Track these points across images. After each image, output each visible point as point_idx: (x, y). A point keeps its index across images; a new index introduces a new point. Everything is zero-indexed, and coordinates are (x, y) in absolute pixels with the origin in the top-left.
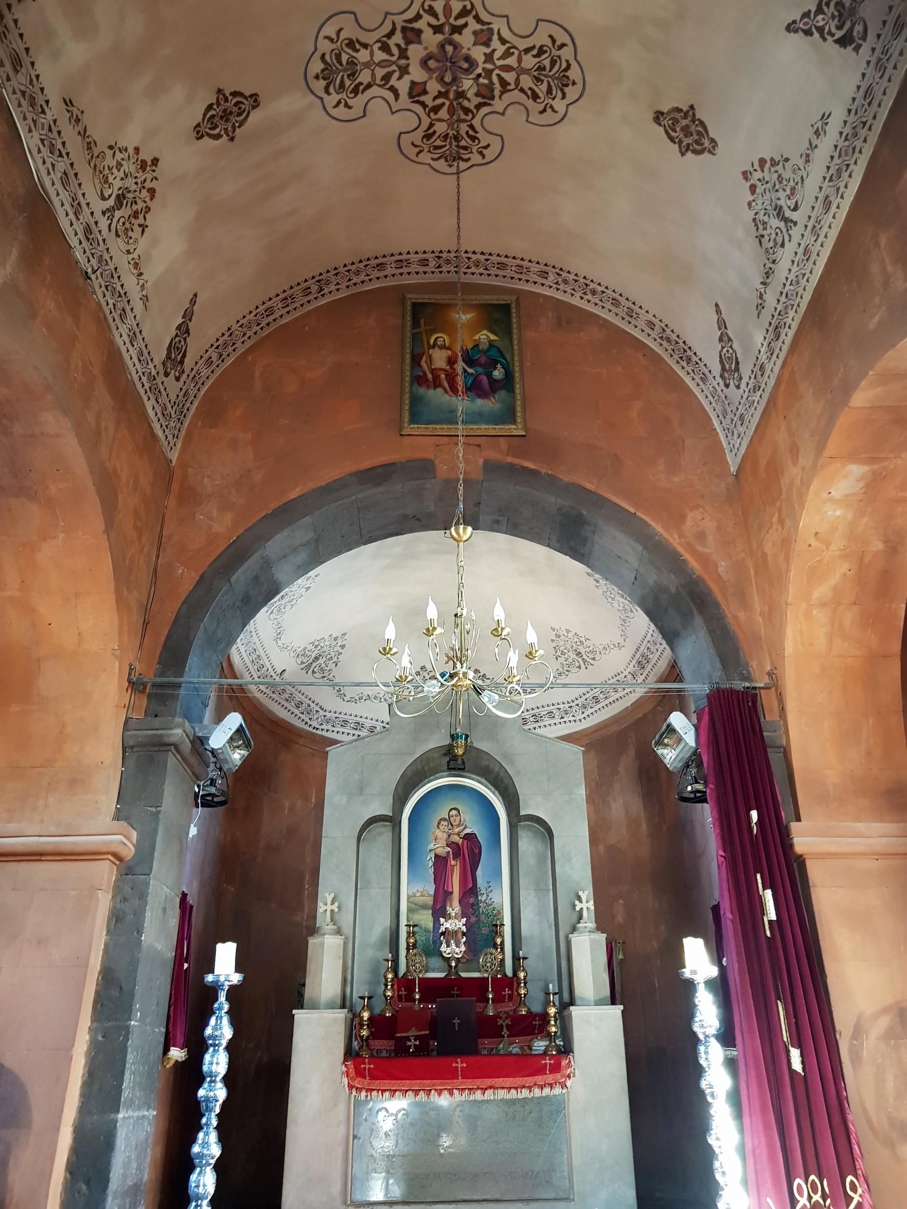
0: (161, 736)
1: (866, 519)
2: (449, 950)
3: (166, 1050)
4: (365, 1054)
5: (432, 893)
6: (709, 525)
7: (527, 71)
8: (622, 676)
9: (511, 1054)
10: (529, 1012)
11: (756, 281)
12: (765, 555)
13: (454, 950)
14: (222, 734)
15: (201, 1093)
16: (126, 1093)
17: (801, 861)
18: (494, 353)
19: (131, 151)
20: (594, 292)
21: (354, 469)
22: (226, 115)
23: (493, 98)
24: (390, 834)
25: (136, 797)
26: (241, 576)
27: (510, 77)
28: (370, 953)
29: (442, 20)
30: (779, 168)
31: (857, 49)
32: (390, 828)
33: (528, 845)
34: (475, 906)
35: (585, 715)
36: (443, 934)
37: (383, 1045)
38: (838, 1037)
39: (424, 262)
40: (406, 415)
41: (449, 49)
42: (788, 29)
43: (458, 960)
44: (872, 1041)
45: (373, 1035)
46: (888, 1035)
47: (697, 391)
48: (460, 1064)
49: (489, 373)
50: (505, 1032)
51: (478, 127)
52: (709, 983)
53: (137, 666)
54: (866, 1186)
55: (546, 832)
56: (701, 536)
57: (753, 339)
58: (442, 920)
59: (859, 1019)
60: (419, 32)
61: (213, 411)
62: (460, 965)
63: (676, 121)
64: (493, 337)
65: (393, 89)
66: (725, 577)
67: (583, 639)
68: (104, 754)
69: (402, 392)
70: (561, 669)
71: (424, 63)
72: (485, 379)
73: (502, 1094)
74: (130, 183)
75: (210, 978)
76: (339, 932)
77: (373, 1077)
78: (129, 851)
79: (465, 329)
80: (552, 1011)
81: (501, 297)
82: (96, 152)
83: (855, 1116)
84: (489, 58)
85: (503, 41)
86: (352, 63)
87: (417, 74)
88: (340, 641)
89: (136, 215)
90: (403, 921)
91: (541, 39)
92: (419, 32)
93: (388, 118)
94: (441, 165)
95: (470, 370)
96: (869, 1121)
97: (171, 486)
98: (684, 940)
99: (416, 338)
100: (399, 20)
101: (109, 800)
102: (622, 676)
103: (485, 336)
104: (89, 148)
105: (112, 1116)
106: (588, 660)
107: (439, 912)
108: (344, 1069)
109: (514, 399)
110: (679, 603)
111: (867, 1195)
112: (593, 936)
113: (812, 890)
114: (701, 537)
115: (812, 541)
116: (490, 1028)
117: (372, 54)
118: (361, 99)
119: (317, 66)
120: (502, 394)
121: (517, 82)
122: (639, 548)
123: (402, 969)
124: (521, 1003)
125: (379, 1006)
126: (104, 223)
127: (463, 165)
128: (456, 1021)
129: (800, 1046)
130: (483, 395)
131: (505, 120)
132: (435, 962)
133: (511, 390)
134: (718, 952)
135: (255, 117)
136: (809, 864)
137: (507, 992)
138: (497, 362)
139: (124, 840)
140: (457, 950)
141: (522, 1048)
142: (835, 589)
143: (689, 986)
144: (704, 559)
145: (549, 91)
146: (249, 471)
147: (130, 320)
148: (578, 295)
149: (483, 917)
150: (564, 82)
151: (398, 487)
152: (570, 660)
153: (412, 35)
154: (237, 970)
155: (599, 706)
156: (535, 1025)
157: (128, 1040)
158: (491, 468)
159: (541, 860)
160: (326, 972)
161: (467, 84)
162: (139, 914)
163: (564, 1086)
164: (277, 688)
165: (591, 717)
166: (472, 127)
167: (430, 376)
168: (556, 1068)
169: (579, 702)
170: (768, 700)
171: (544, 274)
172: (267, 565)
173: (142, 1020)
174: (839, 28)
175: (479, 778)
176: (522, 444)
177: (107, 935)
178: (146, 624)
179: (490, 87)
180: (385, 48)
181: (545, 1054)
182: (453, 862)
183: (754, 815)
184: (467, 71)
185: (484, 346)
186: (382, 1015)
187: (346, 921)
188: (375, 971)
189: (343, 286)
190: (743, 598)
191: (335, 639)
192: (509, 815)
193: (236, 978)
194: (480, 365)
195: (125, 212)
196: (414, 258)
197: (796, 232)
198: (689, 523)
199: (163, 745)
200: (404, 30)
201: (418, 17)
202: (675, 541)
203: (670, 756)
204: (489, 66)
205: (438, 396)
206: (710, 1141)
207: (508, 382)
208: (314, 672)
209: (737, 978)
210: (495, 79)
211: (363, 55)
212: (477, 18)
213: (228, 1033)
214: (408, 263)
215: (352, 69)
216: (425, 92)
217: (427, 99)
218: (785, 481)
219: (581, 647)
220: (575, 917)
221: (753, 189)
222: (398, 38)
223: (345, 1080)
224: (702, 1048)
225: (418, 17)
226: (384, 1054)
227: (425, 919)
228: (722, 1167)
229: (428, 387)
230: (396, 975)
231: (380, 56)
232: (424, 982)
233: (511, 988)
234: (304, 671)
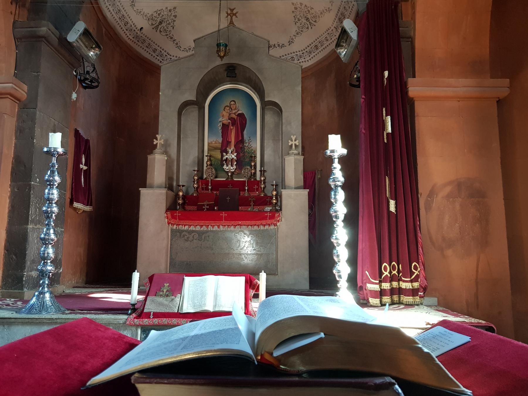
2: (227, 168)
5: (221, 141)
8: (331, 30)
13: (230, 168)
17: (411, 103)
24: (197, 112)
33: (270, 118)
34: (243, 148)
35: (310, 58)
36: (225, 160)
38: (419, 196)
44: (439, 200)
46: (448, 196)
48: (224, 214)
50: (252, 204)
54: (423, 267)
58: (224, 154)
62: (234, 175)
67: (309, 9)
70: (298, 31)
76: (166, 153)
77: (180, 219)
83: (422, 237)
90: (206, 153)
96: (431, 238)
102: (331, 30)
105: (25, 226)
106: (313, 22)
107: (224, 150)
108: (166, 215)
111: (422, 271)
112: (296, 157)
113: (416, 118)
116: (246, 202)
129: (395, 199)
136: (416, 103)
137: (256, 187)
139: (23, 91)
140: (232, 168)
149: (246, 154)
152: (303, 24)
154: (62, 146)
155: (318, 51)
156: (266, 201)
157: (30, 191)
163: (275, 225)
164: (140, 37)
165: (314, 58)
168: (272, 217)
169: (307, 50)
175: (247, 85)
177: (16, 139)
182: (232, 127)
183: (386, 73)
191: (170, 11)
206: (332, 240)
208: (160, 31)
209: (364, 164)
219: (308, 15)
223: (167, 220)
224: (333, 193)
228: (337, 253)
234: (155, 30)
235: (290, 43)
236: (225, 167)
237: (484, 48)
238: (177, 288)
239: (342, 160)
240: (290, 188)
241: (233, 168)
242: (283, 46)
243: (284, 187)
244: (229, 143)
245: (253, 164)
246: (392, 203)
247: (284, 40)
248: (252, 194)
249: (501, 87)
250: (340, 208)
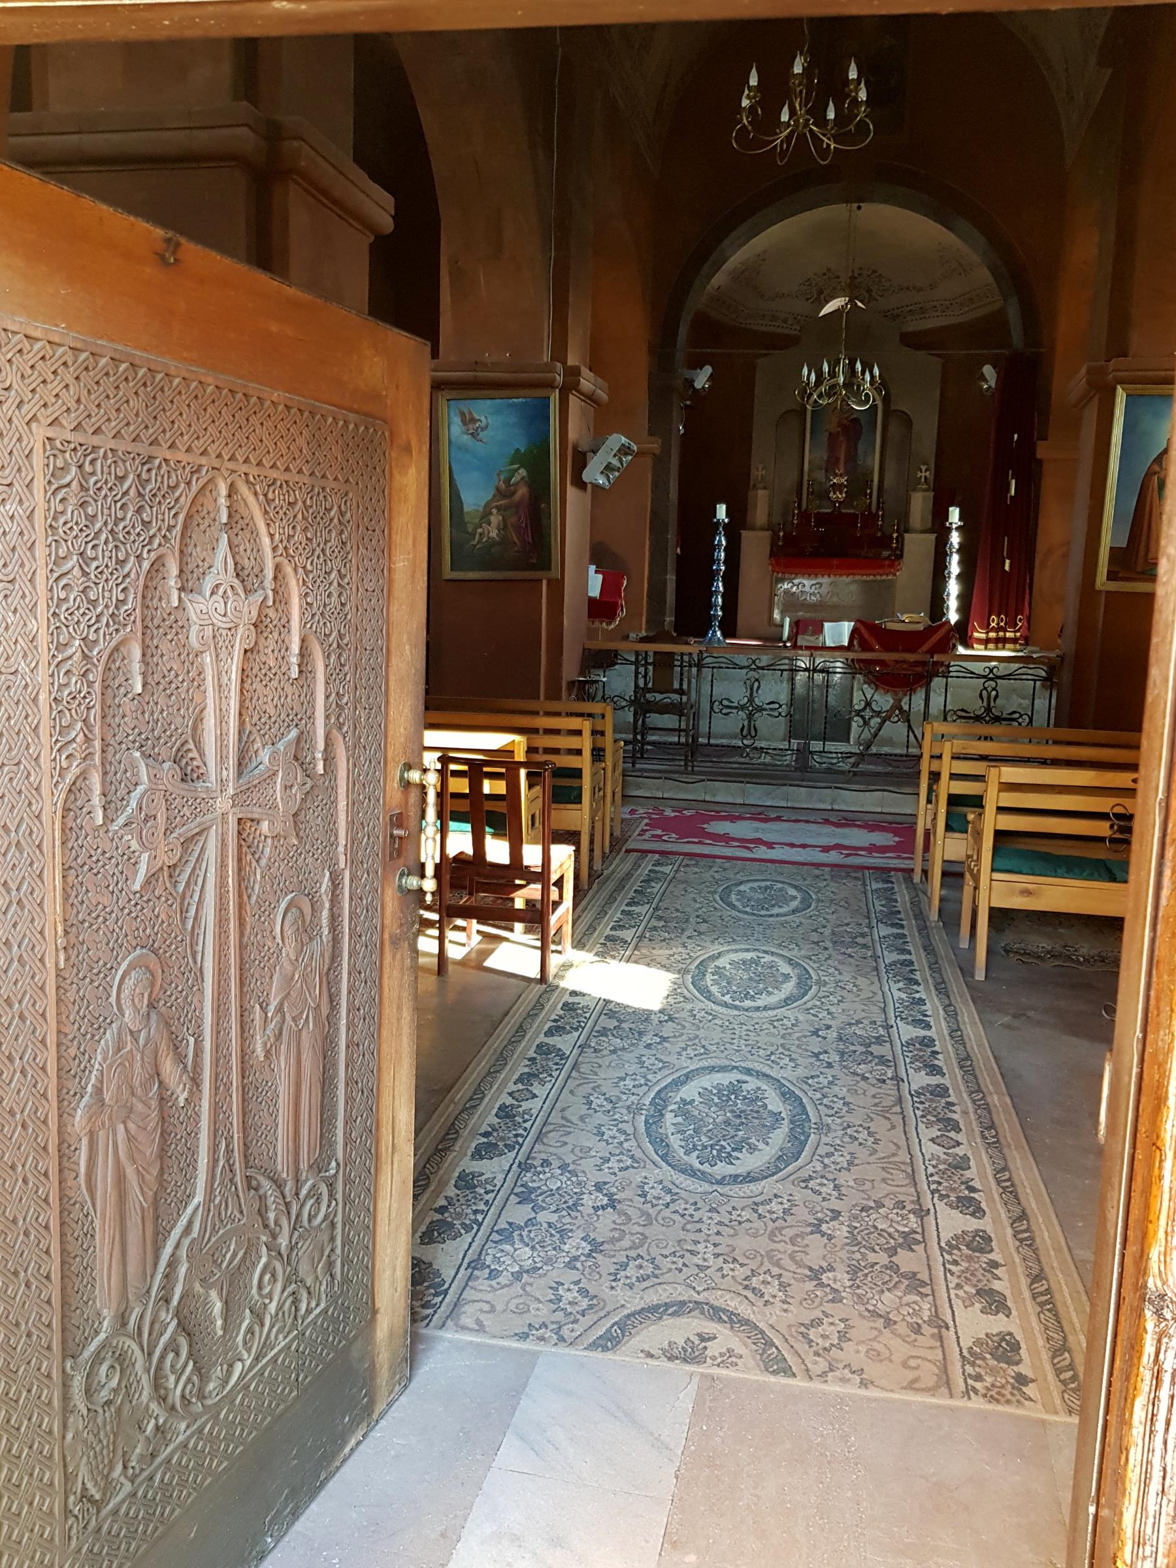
43: (840, 503)
48: (835, 562)
55: (907, 422)
78: (658, 452)
90: (806, 478)
98: (951, 509)
139: (655, 446)
160: (761, 507)
163: (895, 575)
168: (892, 566)
181: (888, 558)
183: (1016, 436)
227: (820, 475)
235: (932, 287)
236: (831, 494)
238: (819, 630)
240: (916, 531)
241: (841, 496)
242: (920, 290)
243: (907, 531)
244: (837, 460)
246: (1008, 562)
250: (954, 568)
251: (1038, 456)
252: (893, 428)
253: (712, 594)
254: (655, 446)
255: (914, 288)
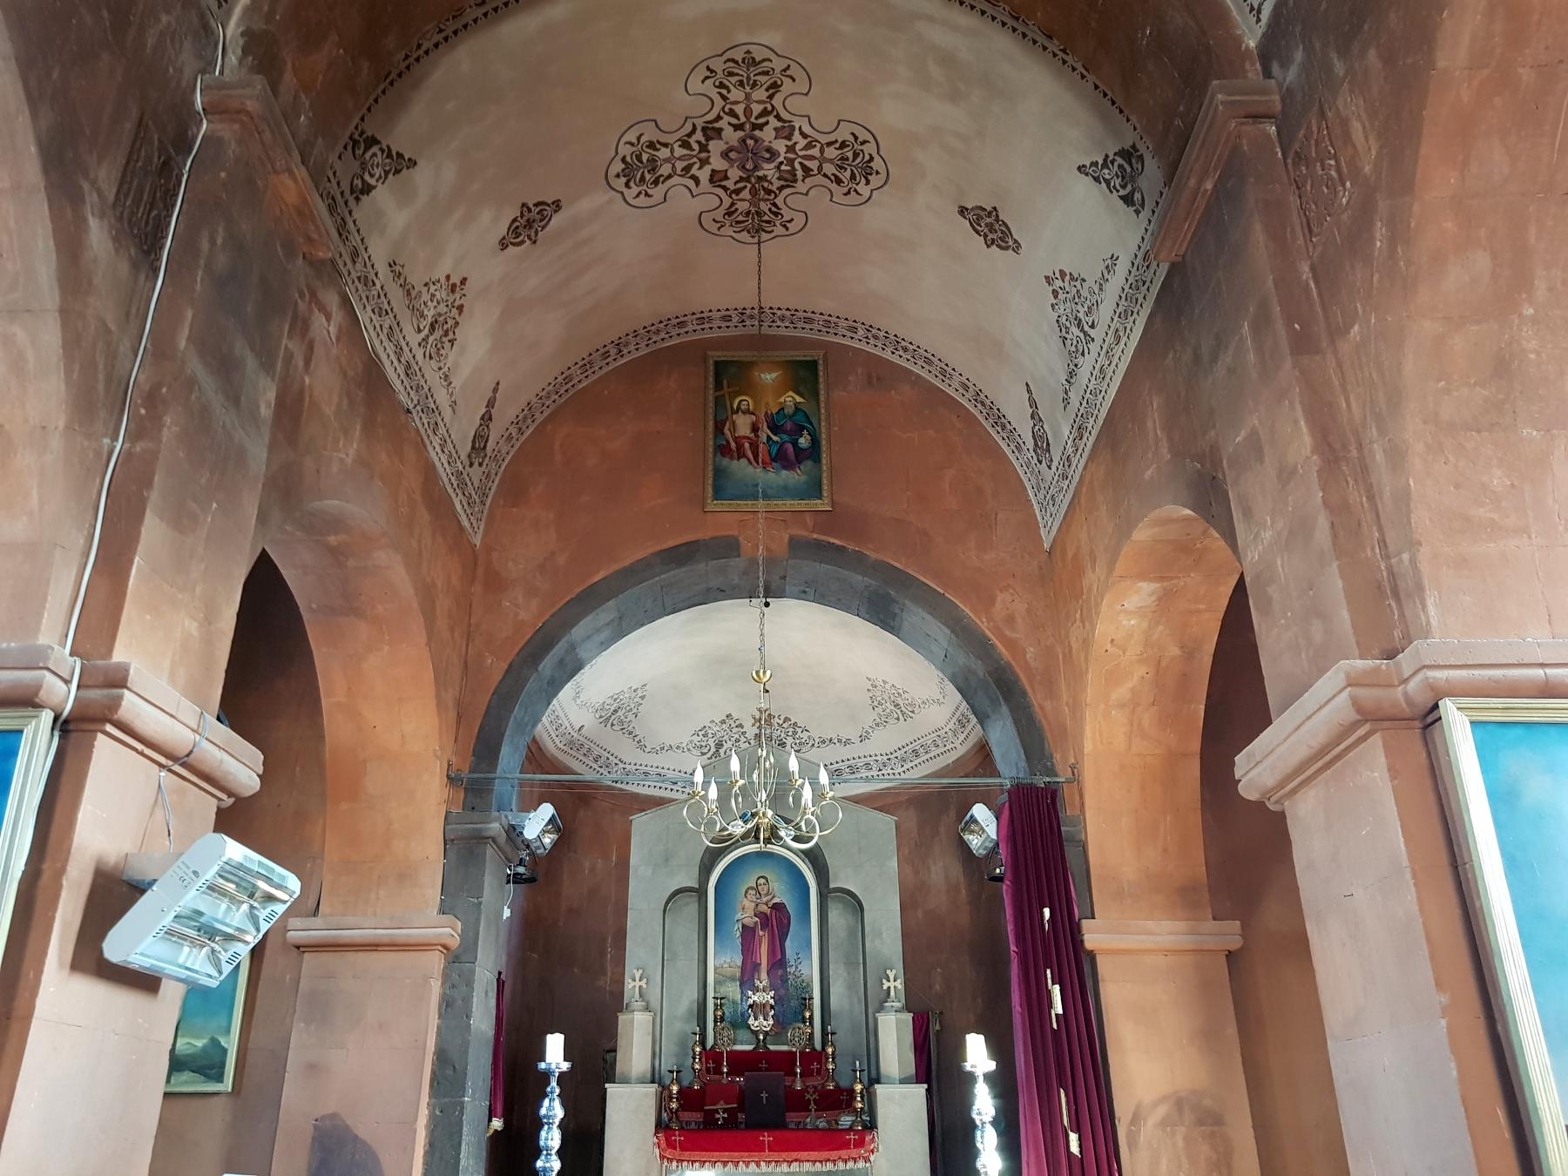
0: (480, 830)
1: (1161, 628)
3: (490, 1120)
4: (674, 1126)
5: (739, 963)
6: (1020, 608)
7: (831, 161)
9: (817, 1129)
10: (837, 1087)
11: (1063, 377)
12: (1070, 647)
13: (762, 1024)
14: (537, 824)
15: (539, 1164)
16: (462, 1162)
17: (1092, 956)
18: (800, 418)
19: (443, 280)
20: (905, 350)
21: (658, 548)
22: (529, 224)
23: (795, 181)
25: (458, 890)
26: (547, 665)
27: (813, 165)
28: (678, 1026)
29: (743, 119)
30: (1078, 284)
31: (1137, 212)
32: (695, 899)
33: (837, 916)
34: (784, 980)
36: (751, 1006)
37: (694, 1117)
39: (727, 318)
40: (710, 489)
41: (750, 142)
42: (1079, 168)
43: (766, 1033)
44: (1149, 1130)
45: (682, 1107)
46: (1163, 1124)
47: (1012, 458)
48: (766, 1138)
49: (793, 442)
50: (812, 1106)
51: (781, 204)
52: (987, 1077)
53: (454, 759)
56: (1010, 620)
57: (1061, 430)
59: (1138, 1107)
60: (720, 130)
61: (514, 490)
63: (979, 218)
64: (799, 399)
65: (694, 178)
66: (1032, 664)
68: (427, 849)
69: (705, 462)
71: (725, 155)
72: (790, 448)
73: (807, 1166)
74: (442, 308)
75: (542, 1066)
76: (647, 1009)
77: (683, 1149)
78: (455, 943)
79: (771, 390)
80: (858, 1087)
81: (807, 352)
82: (414, 294)
84: (791, 149)
85: (805, 136)
86: (652, 160)
87: (717, 163)
88: (640, 693)
89: (446, 333)
90: (711, 994)
91: (843, 134)
92: (720, 130)
93: (686, 201)
94: (744, 236)
95: (775, 438)
97: (480, 574)
99: (719, 402)
100: (700, 123)
101: (433, 894)
103: (791, 399)
104: (409, 294)
109: (820, 469)
110: (992, 685)
114: (1008, 616)
115: (1109, 647)
116: (798, 1102)
117: (672, 152)
118: (662, 188)
119: (618, 167)
120: (809, 464)
121: (820, 168)
122: (947, 631)
123: (710, 1042)
124: (829, 1076)
125: (687, 1078)
126: (419, 353)
127: (764, 236)
128: (764, 1095)
129: (1078, 1130)
130: (788, 465)
131: (811, 200)
132: (743, 1034)
133: (818, 460)
134: (1000, 1048)
135: (557, 221)
136: (1099, 959)
137: (815, 1066)
138: (802, 428)
139: (449, 931)
141: (828, 1122)
142: (1132, 690)
143: (970, 1078)
144: (1011, 644)
145: (853, 177)
146: (553, 553)
147: (442, 430)
148: (889, 350)
149: (791, 990)
150: (868, 172)
151: (702, 566)
153: (712, 132)
156: (840, 1100)
158: (796, 545)
159: (851, 933)
160: (637, 1043)
161: (768, 170)
162: (467, 1000)
163: (867, 1160)
166: (775, 205)
167: (733, 445)
168: (860, 1143)
169: (898, 754)
170: (1067, 792)
171: (854, 330)
172: (572, 647)
173: (473, 1096)
174: (1124, 187)
176: (827, 521)
178: (459, 716)
179: (793, 172)
180: (685, 144)
181: (851, 1129)
183: (1047, 911)
184: (769, 160)
185: (790, 410)
186: (690, 1088)
187: (654, 996)
188: (682, 1044)
189: (643, 345)
190: (1050, 684)
192: (818, 884)
193: (565, 1066)
194: (785, 432)
195: (438, 333)
196: (715, 315)
197: (1094, 347)
198: (998, 605)
199: (480, 839)
200: (704, 129)
201: (719, 118)
202: (984, 626)
203: (975, 841)
204: (791, 156)
205: (742, 469)
207: (814, 452)
210: (797, 166)
211: (664, 153)
212: (778, 117)
213: (559, 1113)
214: (710, 319)
215: (653, 165)
216: (726, 178)
217: (729, 184)
218: (1086, 582)
220: (883, 995)
221: (1055, 294)
222: (699, 136)
224: (978, 1133)
225: (719, 118)
226: (693, 1126)
227: (733, 991)
229: (732, 458)
230: (704, 1048)
231: (679, 152)
232: (733, 1055)
233: (820, 1063)
237: (1197, 865)
239: (988, 1077)
242: (847, 742)
244: (757, 966)
245: (807, 1015)
246: (1073, 1138)
247: (852, 733)
248: (811, 1082)
249: (1229, 934)
250: (984, 1105)
251: (1088, 945)
252: (837, 916)
253: (538, 1124)
254: (449, 931)
255: (840, 741)
